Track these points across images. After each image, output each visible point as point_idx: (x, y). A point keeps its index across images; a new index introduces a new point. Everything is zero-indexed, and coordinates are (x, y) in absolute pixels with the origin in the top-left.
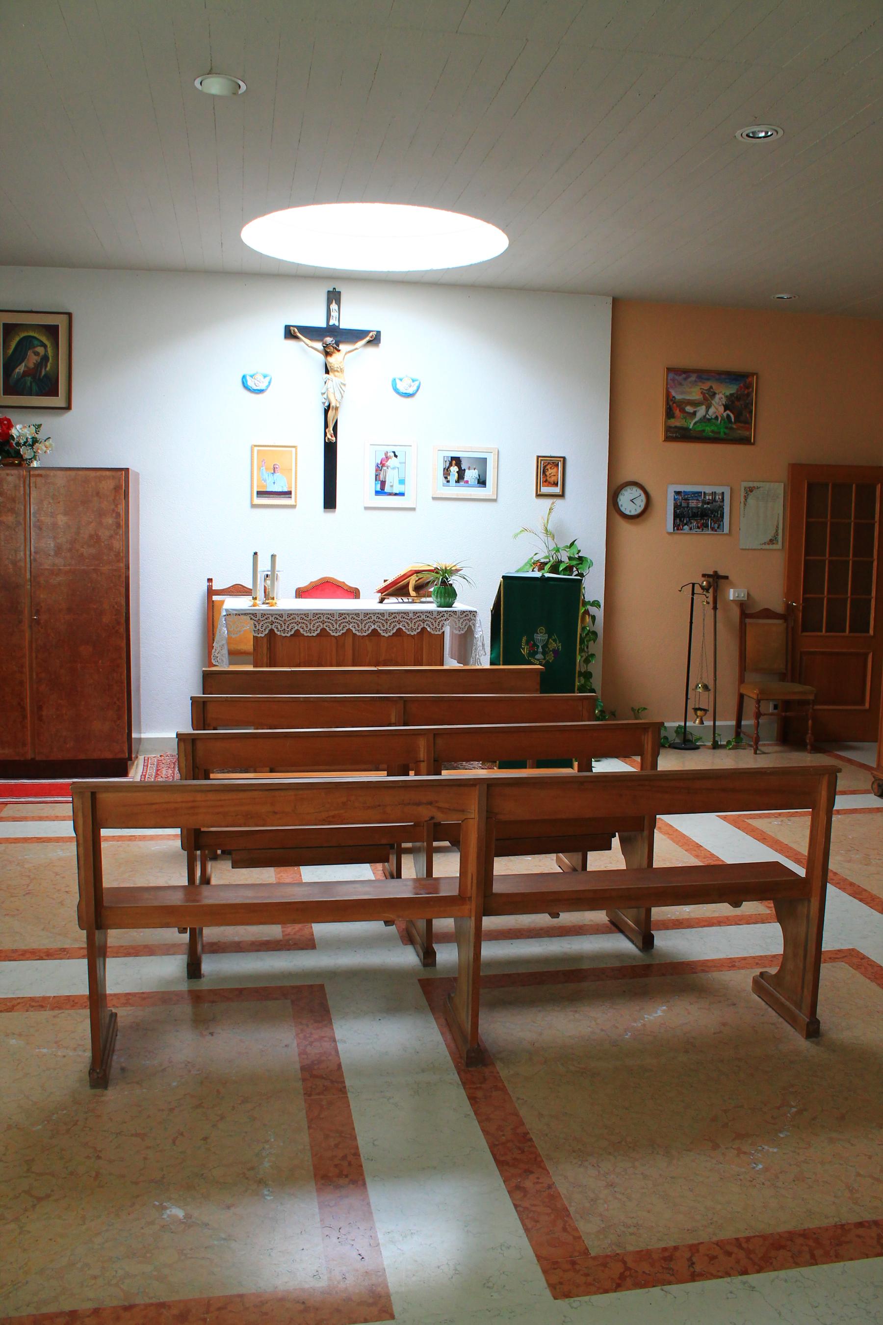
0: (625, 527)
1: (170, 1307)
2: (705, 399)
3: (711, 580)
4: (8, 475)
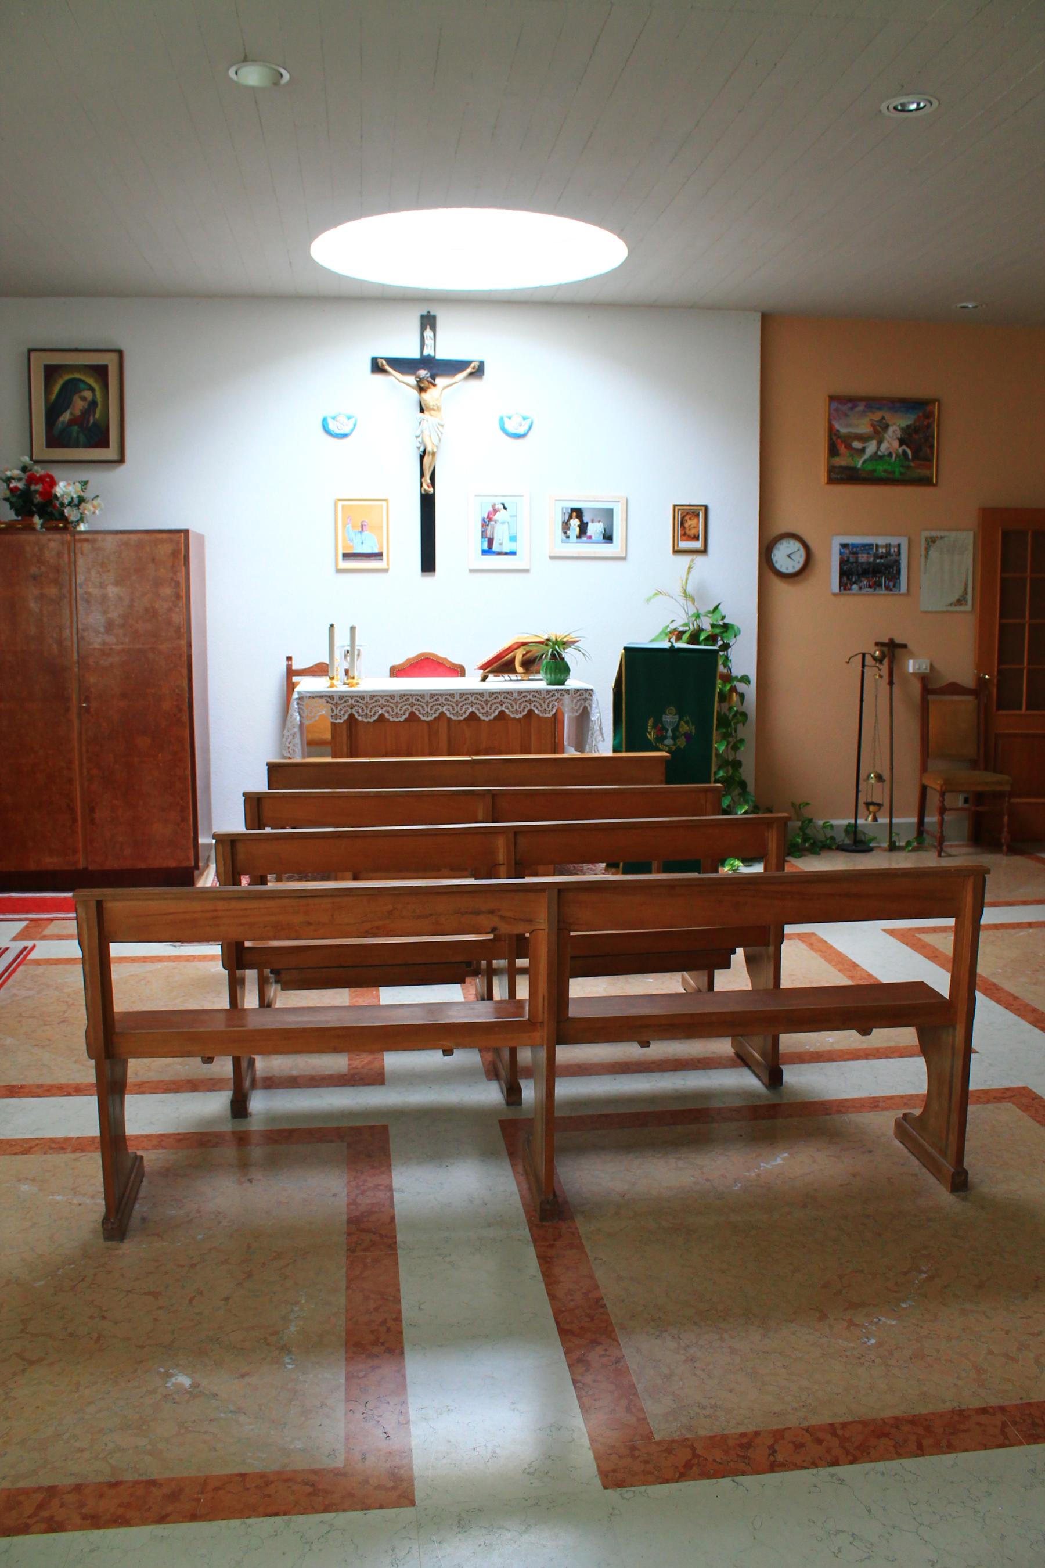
0: (780, 587)
1: (161, 1485)
2: (876, 432)
3: (885, 649)
4: (49, 540)
